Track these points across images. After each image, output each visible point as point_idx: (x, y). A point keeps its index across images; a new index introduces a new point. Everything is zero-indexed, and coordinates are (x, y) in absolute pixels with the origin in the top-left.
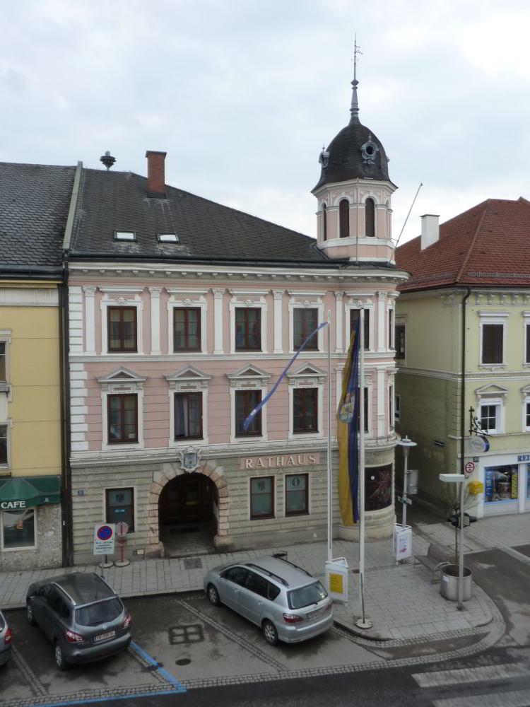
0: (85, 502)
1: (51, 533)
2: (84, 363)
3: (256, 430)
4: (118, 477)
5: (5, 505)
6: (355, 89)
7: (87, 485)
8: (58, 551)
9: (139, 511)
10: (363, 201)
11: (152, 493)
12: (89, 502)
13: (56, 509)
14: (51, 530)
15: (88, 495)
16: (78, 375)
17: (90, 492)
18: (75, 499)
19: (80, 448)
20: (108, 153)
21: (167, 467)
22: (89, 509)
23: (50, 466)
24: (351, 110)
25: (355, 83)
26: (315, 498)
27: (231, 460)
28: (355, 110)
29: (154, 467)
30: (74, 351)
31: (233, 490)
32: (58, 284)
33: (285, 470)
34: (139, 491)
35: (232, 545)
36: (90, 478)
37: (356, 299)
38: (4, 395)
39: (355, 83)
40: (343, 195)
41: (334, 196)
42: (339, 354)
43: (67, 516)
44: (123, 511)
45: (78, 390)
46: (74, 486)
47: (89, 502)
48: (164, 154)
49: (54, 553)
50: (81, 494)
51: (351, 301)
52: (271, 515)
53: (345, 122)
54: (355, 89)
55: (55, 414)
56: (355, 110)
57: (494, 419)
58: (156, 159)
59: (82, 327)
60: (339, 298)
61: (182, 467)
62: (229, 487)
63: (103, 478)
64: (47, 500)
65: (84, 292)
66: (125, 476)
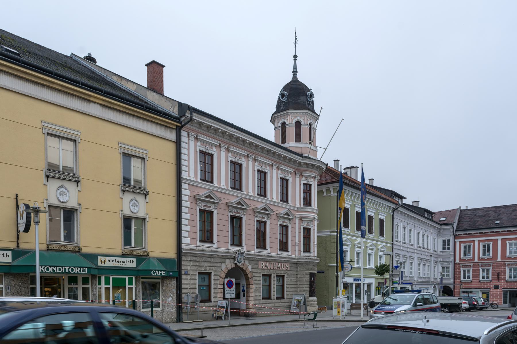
0: (187, 279)
1: (170, 299)
2: (189, 184)
3: (264, 247)
4: (204, 264)
5: (154, 273)
6: (295, 60)
7: (189, 268)
8: (174, 311)
9: (214, 288)
10: (294, 122)
11: (221, 277)
12: (190, 279)
13: (173, 282)
14: (170, 297)
15: (189, 274)
16: (186, 192)
17: (190, 273)
18: (183, 277)
19: (186, 241)
20: (90, 54)
21: (228, 261)
22: (191, 284)
23: (171, 253)
24: (293, 72)
25: (295, 57)
26: (288, 290)
27: (255, 260)
28: (295, 72)
29: (222, 260)
30: (184, 175)
31: (255, 280)
32: (177, 126)
33: (277, 272)
34: (215, 275)
35: (256, 314)
36: (191, 263)
37: (307, 177)
38: (143, 197)
39: (295, 57)
40: (283, 120)
41: (293, 118)
42: (298, 208)
43: (179, 288)
44: (205, 288)
45: (186, 203)
46: (183, 267)
47: (190, 279)
48: (164, 66)
49: (172, 313)
50: (186, 274)
51: (304, 178)
52: (269, 298)
53: (289, 79)
54: (295, 60)
55: (173, 217)
56: (295, 72)
57: (222, 319)
58: (155, 69)
59: (187, 159)
60: (298, 176)
61: (236, 262)
62: (254, 278)
63: (197, 264)
64: (171, 274)
65: (189, 135)
66: (208, 264)
